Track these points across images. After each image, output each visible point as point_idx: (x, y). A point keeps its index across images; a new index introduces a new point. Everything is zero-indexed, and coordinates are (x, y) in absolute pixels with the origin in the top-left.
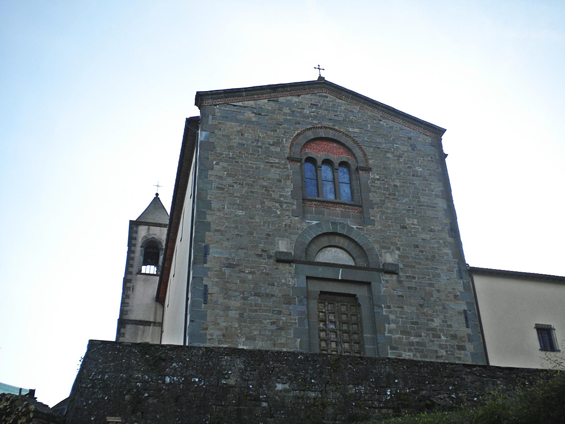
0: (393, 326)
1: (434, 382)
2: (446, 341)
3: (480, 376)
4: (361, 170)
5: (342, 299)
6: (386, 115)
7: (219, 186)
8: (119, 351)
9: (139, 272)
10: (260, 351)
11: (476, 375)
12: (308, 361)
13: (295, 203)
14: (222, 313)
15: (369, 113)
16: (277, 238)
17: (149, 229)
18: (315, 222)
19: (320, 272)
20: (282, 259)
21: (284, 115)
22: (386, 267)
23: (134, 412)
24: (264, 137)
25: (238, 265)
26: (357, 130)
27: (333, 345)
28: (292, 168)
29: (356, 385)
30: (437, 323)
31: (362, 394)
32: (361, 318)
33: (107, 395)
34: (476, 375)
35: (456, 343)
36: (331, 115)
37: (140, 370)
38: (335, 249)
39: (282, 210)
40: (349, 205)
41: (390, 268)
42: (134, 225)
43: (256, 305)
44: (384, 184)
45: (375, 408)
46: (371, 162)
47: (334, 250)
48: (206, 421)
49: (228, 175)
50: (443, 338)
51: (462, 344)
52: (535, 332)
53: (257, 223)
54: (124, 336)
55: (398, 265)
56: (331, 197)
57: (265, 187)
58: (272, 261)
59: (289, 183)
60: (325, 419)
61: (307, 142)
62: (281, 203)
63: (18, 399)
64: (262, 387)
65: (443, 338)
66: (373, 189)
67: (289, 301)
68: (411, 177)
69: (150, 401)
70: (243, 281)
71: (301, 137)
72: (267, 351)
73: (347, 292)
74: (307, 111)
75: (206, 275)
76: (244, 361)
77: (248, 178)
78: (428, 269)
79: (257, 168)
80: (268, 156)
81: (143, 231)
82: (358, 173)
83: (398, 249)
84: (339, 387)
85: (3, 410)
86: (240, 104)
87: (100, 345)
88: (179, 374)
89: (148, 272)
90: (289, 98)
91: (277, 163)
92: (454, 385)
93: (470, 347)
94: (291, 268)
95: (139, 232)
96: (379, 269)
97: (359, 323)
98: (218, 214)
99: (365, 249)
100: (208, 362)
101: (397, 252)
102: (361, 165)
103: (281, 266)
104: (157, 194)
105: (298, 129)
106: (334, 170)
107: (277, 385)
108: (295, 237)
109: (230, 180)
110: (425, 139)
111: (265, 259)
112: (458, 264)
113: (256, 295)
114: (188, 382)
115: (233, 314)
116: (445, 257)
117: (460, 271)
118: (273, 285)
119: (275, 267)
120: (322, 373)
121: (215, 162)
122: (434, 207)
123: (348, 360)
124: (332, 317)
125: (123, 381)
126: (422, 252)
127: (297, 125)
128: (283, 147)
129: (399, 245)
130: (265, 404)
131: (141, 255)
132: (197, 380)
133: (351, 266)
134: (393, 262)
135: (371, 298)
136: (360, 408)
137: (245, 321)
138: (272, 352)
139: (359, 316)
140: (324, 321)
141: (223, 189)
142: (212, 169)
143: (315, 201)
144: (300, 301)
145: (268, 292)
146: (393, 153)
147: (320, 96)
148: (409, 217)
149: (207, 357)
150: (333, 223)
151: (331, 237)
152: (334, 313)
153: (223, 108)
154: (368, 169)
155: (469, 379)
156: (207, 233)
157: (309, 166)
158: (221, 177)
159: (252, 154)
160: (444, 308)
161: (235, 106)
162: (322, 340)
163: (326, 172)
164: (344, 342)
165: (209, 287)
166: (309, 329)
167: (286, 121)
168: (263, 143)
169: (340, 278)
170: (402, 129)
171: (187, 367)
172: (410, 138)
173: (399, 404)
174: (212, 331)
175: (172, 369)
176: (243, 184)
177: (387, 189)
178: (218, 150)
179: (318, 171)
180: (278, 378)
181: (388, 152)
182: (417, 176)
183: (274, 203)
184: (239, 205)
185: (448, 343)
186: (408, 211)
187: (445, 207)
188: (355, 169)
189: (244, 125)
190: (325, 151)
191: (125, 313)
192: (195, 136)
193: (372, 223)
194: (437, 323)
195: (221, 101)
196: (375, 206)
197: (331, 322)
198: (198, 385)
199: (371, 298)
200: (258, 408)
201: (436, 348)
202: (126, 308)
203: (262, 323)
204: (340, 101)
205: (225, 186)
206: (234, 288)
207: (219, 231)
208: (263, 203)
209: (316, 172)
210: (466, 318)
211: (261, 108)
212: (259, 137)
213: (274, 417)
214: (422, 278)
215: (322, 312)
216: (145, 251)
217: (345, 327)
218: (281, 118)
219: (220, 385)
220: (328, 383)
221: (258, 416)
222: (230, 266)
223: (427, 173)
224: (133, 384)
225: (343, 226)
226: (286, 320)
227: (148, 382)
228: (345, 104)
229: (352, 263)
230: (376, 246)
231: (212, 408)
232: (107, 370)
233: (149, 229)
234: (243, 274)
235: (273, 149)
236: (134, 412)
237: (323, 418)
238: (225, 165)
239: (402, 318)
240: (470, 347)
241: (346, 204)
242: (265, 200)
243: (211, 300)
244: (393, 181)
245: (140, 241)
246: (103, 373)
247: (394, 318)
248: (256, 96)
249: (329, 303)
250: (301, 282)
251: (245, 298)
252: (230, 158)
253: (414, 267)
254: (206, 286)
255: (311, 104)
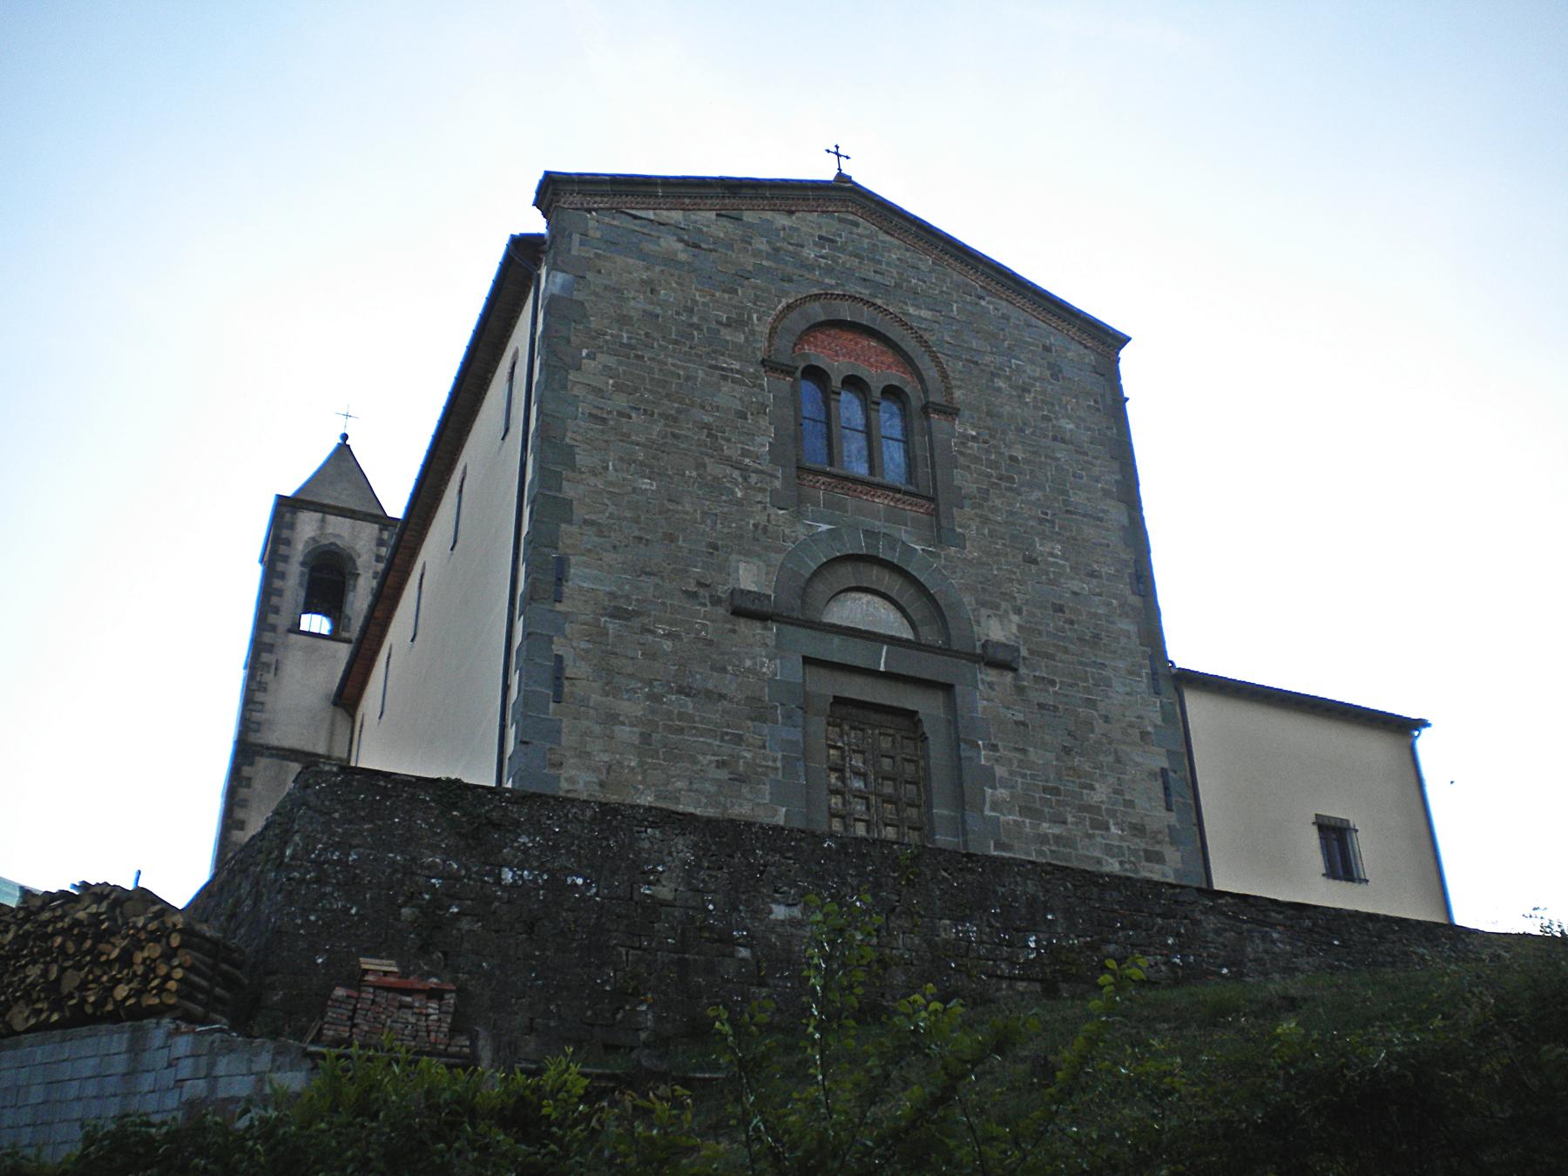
0: (1002, 793)
1: (1134, 926)
2: (1121, 838)
3: (1235, 918)
4: (935, 411)
5: (885, 717)
6: (993, 286)
7: (595, 411)
8: (386, 794)
9: (295, 628)
10: (732, 821)
11: (1224, 914)
12: (847, 854)
13: (779, 474)
14: (597, 729)
15: (955, 276)
16: (734, 557)
17: (323, 520)
18: (824, 527)
19: (835, 649)
20: (746, 609)
21: (754, 255)
22: (990, 651)
23: (424, 949)
24: (704, 304)
25: (637, 614)
26: (925, 313)
27: (861, 830)
28: (772, 388)
29: (958, 920)
30: (1100, 794)
31: (970, 942)
32: (927, 769)
33: (354, 903)
34: (1224, 914)
35: (1143, 845)
36: (867, 271)
37: (438, 846)
38: (869, 597)
39: (748, 487)
40: (906, 493)
41: (1001, 655)
42: (286, 508)
43: (681, 716)
44: (988, 451)
45: (1001, 977)
46: (957, 394)
47: (866, 598)
48: (604, 983)
49: (618, 388)
50: (1113, 829)
51: (1157, 848)
52: (1314, 835)
53: (687, 513)
54: (249, 786)
55: (1018, 650)
56: (861, 469)
57: (707, 426)
58: (721, 610)
59: (764, 422)
60: (888, 997)
61: (809, 329)
62: (744, 470)
63: (129, 899)
64: (736, 909)
65: (1113, 829)
66: (961, 460)
67: (760, 713)
68: (1049, 442)
69: (465, 924)
70: (651, 655)
71: (794, 315)
72: (749, 825)
73: (900, 705)
74: (810, 253)
75: (560, 631)
76: (695, 845)
77: (665, 401)
78: (1086, 665)
79: (688, 378)
80: (714, 352)
81: (307, 526)
82: (928, 418)
83: (1018, 611)
84: (919, 922)
85: (90, 925)
86: (650, 215)
87: (337, 775)
88: (535, 864)
89: (315, 630)
90: (768, 215)
91: (738, 372)
92: (1178, 935)
93: (1173, 856)
94: (768, 633)
95: (299, 527)
96: (974, 655)
97: (922, 781)
98: (592, 481)
99: (942, 603)
100: (607, 839)
101: (1015, 618)
102: (935, 398)
103: (743, 626)
104: (345, 437)
105: (787, 294)
106: (868, 405)
107: (774, 906)
108: (778, 558)
109: (621, 401)
110: (1075, 353)
111: (705, 605)
112: (1151, 658)
113: (681, 691)
114: (557, 885)
115: (625, 733)
116: (1123, 641)
117: (1154, 676)
118: (724, 670)
119: (729, 626)
120: (881, 886)
121: (584, 352)
122: (1101, 520)
123: (940, 858)
124: (857, 761)
125: (396, 871)
126: (1072, 622)
127: (786, 285)
128: (753, 333)
129: (1019, 602)
130: (744, 953)
131: (301, 584)
132: (580, 881)
133: (908, 641)
134: (1004, 640)
135: (953, 723)
136: (969, 976)
137: (655, 754)
138: (761, 827)
139: (922, 763)
140: (839, 770)
141: (604, 421)
142: (579, 369)
143: (827, 474)
144: (788, 716)
145: (710, 686)
146: (1009, 378)
147: (841, 220)
148: (1043, 536)
149: (604, 826)
150: (869, 533)
151: (863, 565)
152: (862, 752)
153: (607, 220)
154: (951, 412)
155: (1211, 923)
156: (563, 526)
157: (808, 388)
158: (601, 390)
159: (676, 342)
160: (1118, 761)
161: (635, 217)
162: (834, 816)
163: (850, 408)
164: (886, 825)
165: (568, 661)
166: (807, 786)
167: (761, 270)
168: (702, 318)
169: (882, 668)
170: (1029, 326)
171: (555, 848)
172: (1047, 349)
173: (1055, 971)
174: (573, 772)
175: (518, 849)
176: (652, 414)
177: (993, 465)
178: (594, 322)
179: (833, 404)
180: (776, 891)
181: (998, 376)
182: (1063, 441)
183: (728, 470)
184: (642, 464)
185: (1125, 844)
186: (1041, 521)
187: (1125, 521)
188: (920, 408)
189: (657, 269)
190: (849, 354)
191: (254, 726)
192: (530, 279)
193: (960, 542)
194: (1100, 794)
195: (604, 202)
196: (967, 502)
197: (857, 774)
198: (582, 895)
199: (953, 723)
200: (728, 960)
201: (1097, 854)
202: (256, 716)
203: (695, 762)
204: (888, 238)
205: (609, 413)
206: (630, 670)
207: (592, 523)
208: (700, 466)
209: (826, 403)
210: (1166, 788)
211: (700, 231)
212: (694, 301)
213: (766, 985)
214: (1071, 685)
215: (835, 747)
216: (311, 575)
217: (888, 788)
218: (749, 262)
219: (636, 898)
220: (893, 909)
221: (728, 981)
222: (618, 614)
223: (1085, 437)
224: (421, 880)
225: (893, 542)
226: (754, 759)
227: (459, 879)
228: (899, 248)
229: (907, 634)
230: (968, 599)
231: (620, 954)
232: (355, 842)
233: (323, 520)
234: (650, 638)
235: (727, 334)
236: (424, 949)
237: (883, 995)
238: (611, 361)
239: (1024, 776)
240: (1173, 856)
241: (899, 491)
242: (707, 460)
243: (572, 693)
244: (1008, 446)
245: (299, 550)
246: (344, 846)
247: (1006, 775)
248: (687, 201)
249: (853, 728)
250: (790, 670)
251: (654, 698)
252: (622, 345)
253: (1052, 657)
254: (559, 658)
255: (820, 237)
